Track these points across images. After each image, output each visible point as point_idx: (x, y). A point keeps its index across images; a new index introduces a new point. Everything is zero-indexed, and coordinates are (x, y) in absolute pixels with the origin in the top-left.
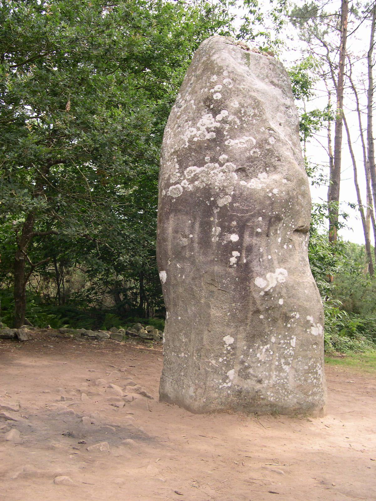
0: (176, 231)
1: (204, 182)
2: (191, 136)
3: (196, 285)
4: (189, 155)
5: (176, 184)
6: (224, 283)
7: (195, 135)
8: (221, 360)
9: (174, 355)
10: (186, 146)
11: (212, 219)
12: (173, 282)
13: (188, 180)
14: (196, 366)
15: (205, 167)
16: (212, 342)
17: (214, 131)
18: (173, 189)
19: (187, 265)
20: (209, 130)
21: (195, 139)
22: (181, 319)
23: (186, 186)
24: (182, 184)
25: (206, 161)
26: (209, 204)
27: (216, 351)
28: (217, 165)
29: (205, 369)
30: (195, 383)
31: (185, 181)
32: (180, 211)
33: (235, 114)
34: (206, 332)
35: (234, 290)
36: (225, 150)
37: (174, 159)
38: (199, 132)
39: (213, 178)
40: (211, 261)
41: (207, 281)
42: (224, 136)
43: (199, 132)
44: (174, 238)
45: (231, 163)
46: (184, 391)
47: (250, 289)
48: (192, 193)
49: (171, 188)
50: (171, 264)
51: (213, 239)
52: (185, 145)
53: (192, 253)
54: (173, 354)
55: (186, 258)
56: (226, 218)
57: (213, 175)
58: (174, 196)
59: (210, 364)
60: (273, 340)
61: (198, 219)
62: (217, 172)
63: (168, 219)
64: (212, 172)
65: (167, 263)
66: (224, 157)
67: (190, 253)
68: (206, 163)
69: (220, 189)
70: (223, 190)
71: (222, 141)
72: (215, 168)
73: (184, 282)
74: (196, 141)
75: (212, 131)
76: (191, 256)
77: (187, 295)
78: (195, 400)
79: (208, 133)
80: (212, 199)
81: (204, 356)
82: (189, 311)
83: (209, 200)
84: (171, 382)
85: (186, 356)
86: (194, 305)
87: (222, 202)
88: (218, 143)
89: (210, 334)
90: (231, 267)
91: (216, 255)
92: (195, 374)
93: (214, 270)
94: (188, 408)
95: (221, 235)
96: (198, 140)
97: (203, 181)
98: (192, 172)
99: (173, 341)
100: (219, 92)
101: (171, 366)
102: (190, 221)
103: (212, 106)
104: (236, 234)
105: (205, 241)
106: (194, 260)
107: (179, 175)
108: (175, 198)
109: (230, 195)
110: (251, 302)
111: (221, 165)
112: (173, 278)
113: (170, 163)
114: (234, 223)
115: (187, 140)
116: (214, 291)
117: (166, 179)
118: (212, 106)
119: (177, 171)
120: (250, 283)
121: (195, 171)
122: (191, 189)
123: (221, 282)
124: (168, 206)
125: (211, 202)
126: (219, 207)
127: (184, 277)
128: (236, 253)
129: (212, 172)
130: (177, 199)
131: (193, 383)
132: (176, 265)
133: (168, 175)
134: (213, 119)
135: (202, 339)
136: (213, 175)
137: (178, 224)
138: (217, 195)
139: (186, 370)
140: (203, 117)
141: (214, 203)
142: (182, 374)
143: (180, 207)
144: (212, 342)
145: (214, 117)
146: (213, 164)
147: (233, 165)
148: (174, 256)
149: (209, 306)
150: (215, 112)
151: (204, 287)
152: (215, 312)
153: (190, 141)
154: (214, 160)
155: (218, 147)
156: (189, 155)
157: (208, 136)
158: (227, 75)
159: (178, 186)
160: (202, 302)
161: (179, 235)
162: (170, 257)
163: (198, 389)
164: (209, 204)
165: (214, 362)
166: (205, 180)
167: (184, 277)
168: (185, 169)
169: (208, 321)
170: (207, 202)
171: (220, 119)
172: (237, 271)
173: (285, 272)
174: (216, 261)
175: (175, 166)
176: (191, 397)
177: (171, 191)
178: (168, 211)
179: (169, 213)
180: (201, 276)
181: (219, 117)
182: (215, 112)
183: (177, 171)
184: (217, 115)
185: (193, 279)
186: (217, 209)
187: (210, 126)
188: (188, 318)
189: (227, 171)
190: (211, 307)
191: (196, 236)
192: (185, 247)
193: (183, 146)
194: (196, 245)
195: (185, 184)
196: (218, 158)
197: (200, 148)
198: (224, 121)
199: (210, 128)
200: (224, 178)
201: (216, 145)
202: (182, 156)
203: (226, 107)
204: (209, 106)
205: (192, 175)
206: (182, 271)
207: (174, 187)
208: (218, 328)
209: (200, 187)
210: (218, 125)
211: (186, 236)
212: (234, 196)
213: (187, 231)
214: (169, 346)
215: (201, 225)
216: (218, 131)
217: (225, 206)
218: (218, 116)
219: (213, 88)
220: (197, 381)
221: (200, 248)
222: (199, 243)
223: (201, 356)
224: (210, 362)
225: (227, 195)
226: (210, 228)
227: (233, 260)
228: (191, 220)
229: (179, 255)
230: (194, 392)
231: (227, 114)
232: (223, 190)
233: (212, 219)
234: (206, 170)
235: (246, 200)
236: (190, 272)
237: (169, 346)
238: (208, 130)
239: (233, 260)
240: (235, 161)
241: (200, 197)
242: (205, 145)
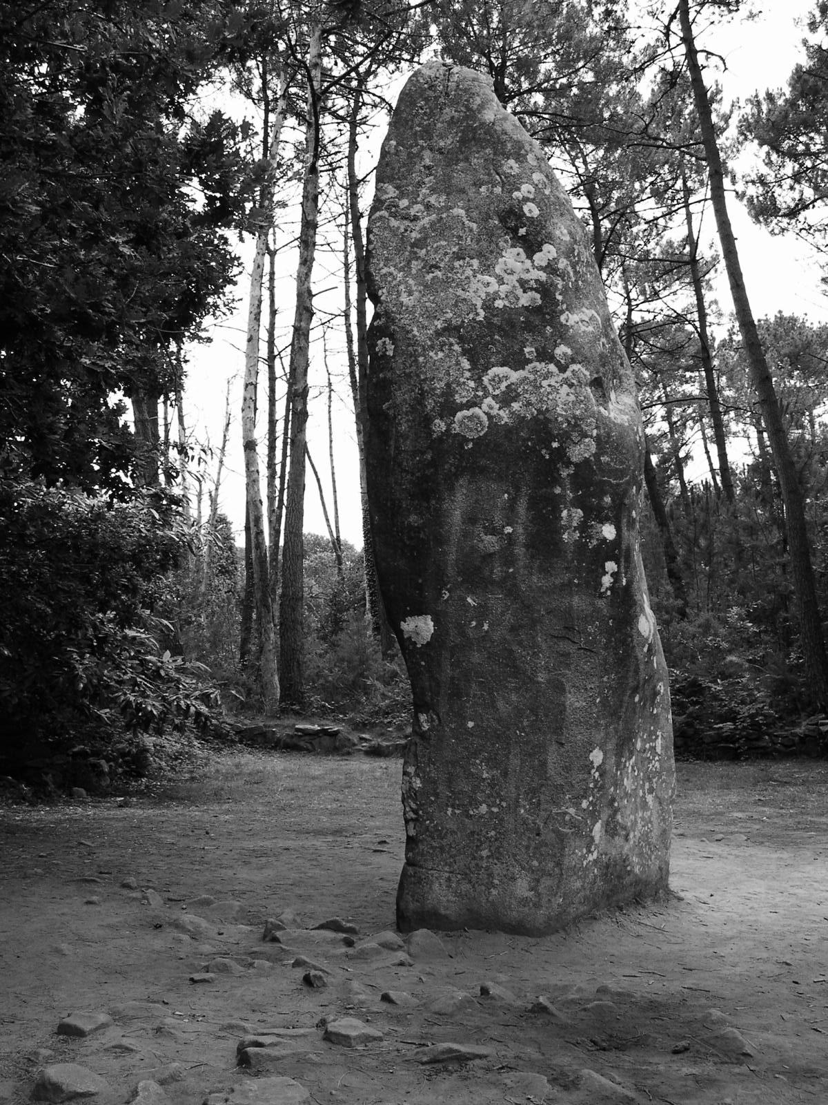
0: (471, 519)
1: (531, 404)
2: (488, 294)
3: (520, 643)
4: (488, 339)
5: (471, 407)
6: (590, 634)
7: (496, 293)
8: (585, 804)
9: (453, 814)
10: (480, 318)
11: (558, 490)
12: (453, 638)
13: (494, 397)
14: (528, 829)
15: (526, 371)
16: (567, 769)
17: (536, 290)
18: (465, 417)
19: (496, 600)
20: (526, 286)
21: (499, 304)
22: (476, 726)
23: (494, 412)
24: (484, 407)
25: (527, 356)
26: (547, 457)
27: (576, 786)
28: (552, 367)
29: (556, 831)
30: (531, 867)
31: (489, 400)
32: (483, 470)
33: (568, 257)
34: (554, 747)
35: (606, 648)
36: (562, 334)
37: (451, 345)
38: (504, 288)
39: (550, 397)
40: (563, 585)
41: (552, 632)
42: (557, 303)
43: (504, 288)
44: (466, 535)
45: (579, 366)
46: (494, 892)
47: (632, 641)
48: (509, 431)
49: (459, 415)
50: (450, 597)
51: (565, 536)
52: (477, 314)
53: (511, 570)
54: (449, 813)
55: (493, 582)
56: (592, 489)
57: (549, 389)
58: (470, 435)
59: (567, 818)
60: (639, 745)
61: (524, 489)
62: (557, 385)
63: (451, 489)
64: (545, 383)
65: (440, 595)
66: (562, 350)
67: (505, 568)
68: (529, 361)
69: (569, 423)
70: (576, 424)
71: (555, 315)
72: (548, 375)
73: (486, 637)
74: (501, 307)
75: (532, 289)
76: (507, 577)
77: (496, 667)
78: (537, 906)
79: (525, 292)
80: (555, 445)
81: (547, 802)
82: (500, 704)
83: (549, 447)
84: (449, 879)
85: (495, 810)
86: (517, 690)
87: (581, 451)
88: (548, 317)
89: (563, 750)
90: (601, 596)
91: (578, 572)
92: (527, 847)
93: (571, 607)
94: (517, 929)
95: (584, 527)
96: (505, 306)
97: (529, 404)
98: (500, 381)
99: (450, 781)
100: (533, 201)
101: (444, 842)
102: (506, 495)
103: (522, 231)
104: (611, 524)
105: (544, 538)
106: (515, 585)
107: (472, 384)
108: (472, 440)
109: (591, 437)
110: (632, 668)
111: (563, 369)
112: (453, 632)
113: (441, 355)
114: (608, 499)
115: (479, 303)
116: (570, 653)
117: (438, 392)
118: (522, 231)
119: (468, 374)
120: (632, 628)
121: (507, 378)
122: (506, 420)
123: (584, 631)
124: (455, 458)
125: (552, 451)
126: (572, 463)
127: (486, 627)
128: (611, 566)
129: (545, 383)
130: (478, 442)
131: (523, 868)
132: (464, 599)
133: (443, 384)
134: (528, 262)
135: (544, 764)
136: (549, 389)
137: (477, 501)
138: (565, 437)
139: (497, 844)
140: (504, 254)
141: (561, 456)
142: (485, 853)
143: (483, 462)
144: (567, 769)
145: (530, 256)
146: (543, 364)
147: (583, 370)
148: (460, 579)
149: (559, 688)
150: (531, 246)
151: (544, 646)
152: (574, 701)
153: (488, 306)
154: (545, 355)
155: (548, 328)
156: (488, 339)
157: (525, 299)
158: (535, 163)
159: (476, 410)
160: (540, 679)
161: (479, 529)
162: (449, 582)
163: (543, 880)
164: (547, 457)
165: (572, 811)
166: (533, 400)
167: (486, 627)
168: (483, 371)
169: (557, 722)
170: (543, 452)
171: (544, 264)
172: (612, 604)
173: (492, 550)
174: (577, 585)
175: (458, 363)
176: (524, 902)
177: (461, 423)
178: (453, 469)
179: (456, 476)
180: (534, 622)
181: (541, 258)
182: (531, 246)
183: (468, 374)
184: (534, 253)
185: (513, 629)
186: (567, 467)
187: (526, 276)
188: (499, 721)
189: (574, 381)
190: (567, 689)
191: (521, 530)
192: (491, 555)
193: (471, 316)
194: (520, 551)
195: (491, 408)
196: (553, 351)
197: (512, 324)
198: (551, 268)
199: (527, 282)
200: (572, 398)
201: (546, 323)
202: (471, 340)
203: (549, 239)
204: (514, 231)
205: (503, 386)
206: (482, 612)
207: (465, 413)
208: (578, 735)
209: (525, 417)
210: (543, 276)
211: (493, 531)
212: (598, 439)
213: (498, 519)
214: (437, 795)
215: (533, 504)
216: (545, 290)
217: (587, 460)
218: (537, 256)
219: (518, 189)
220: (535, 863)
221: (532, 557)
222: (527, 546)
223: (539, 803)
224: (566, 813)
225: (586, 436)
226: (556, 512)
227: (607, 580)
228: (509, 494)
229: (474, 573)
230: (532, 889)
231: (555, 255)
232: (576, 425)
233: (558, 490)
234: (532, 377)
235: (616, 448)
236: (503, 614)
237: (437, 795)
238: (523, 284)
239: (607, 580)
240: (585, 361)
241: (529, 439)
242: (522, 319)
